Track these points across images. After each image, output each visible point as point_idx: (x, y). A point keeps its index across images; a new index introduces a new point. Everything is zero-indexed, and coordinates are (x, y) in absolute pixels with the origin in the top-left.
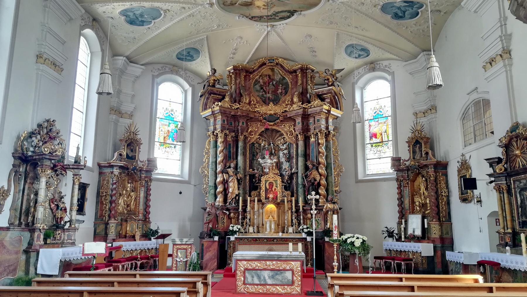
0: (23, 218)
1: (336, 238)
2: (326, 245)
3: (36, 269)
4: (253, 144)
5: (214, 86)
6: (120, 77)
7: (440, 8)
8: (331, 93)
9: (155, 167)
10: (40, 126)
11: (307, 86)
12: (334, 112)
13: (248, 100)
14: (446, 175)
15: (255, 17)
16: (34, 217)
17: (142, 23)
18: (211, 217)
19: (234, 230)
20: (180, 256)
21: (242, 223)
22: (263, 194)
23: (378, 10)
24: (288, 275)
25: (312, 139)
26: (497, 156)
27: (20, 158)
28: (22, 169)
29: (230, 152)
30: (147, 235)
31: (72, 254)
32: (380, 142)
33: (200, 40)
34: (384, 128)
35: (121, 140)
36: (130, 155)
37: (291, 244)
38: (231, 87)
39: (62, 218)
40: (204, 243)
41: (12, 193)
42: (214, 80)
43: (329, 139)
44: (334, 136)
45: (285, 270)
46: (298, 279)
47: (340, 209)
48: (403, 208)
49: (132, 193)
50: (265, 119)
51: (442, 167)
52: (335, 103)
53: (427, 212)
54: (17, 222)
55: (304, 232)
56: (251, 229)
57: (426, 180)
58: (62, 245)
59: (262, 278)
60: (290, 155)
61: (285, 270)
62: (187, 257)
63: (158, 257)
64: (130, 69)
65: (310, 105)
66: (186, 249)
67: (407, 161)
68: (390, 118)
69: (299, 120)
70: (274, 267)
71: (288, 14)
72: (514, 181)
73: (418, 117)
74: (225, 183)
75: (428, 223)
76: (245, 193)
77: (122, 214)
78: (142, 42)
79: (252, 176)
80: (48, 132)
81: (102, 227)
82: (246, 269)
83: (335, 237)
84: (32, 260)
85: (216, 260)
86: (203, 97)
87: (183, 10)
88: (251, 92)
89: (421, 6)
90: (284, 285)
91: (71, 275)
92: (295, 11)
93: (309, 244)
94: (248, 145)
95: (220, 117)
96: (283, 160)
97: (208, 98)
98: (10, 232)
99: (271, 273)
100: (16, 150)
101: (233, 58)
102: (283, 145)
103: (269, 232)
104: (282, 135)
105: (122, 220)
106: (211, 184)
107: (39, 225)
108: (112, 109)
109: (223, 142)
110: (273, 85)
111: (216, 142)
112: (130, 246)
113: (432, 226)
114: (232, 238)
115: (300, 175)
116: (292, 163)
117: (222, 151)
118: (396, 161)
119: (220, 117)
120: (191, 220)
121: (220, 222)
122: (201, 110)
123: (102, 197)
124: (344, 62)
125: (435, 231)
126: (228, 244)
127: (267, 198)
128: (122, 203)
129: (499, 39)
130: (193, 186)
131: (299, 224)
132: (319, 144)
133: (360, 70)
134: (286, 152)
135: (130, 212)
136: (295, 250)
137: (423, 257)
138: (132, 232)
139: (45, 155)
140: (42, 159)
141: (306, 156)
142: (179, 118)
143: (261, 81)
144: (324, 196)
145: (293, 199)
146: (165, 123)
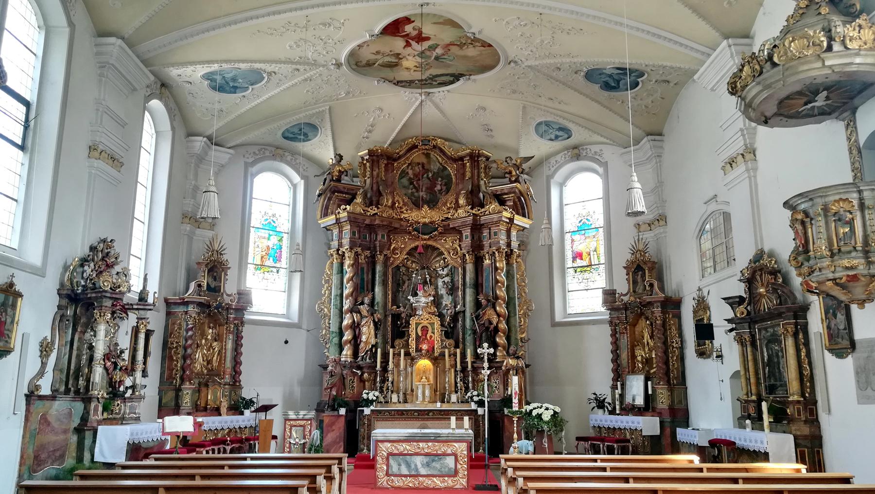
0: (71, 382)
1: (517, 409)
2: (506, 420)
3: (93, 456)
4: (398, 268)
5: (339, 180)
6: (197, 166)
7: (667, 78)
8: (514, 192)
9: (249, 303)
10: (93, 249)
11: (479, 182)
12: (519, 220)
13: (390, 202)
14: (678, 317)
15: (402, 82)
16: (88, 380)
17: (234, 90)
18: (335, 379)
19: (370, 398)
20: (296, 437)
21: (381, 388)
22: (413, 344)
23: (581, 77)
24: (450, 461)
25: (487, 262)
26: (738, 295)
27: (68, 297)
28: (69, 312)
29: (362, 280)
30: (237, 408)
31: (142, 434)
32: (587, 266)
33: (320, 112)
34: (593, 245)
35: (198, 263)
36: (212, 286)
37: (453, 418)
38: (365, 181)
39: (121, 382)
40: (325, 419)
41: (56, 346)
42: (340, 171)
43: (511, 261)
44: (519, 256)
45: (445, 454)
46: (463, 467)
47: (527, 366)
48: (619, 366)
49: (215, 344)
50: (415, 230)
51: (673, 305)
52: (521, 208)
53: (652, 371)
54: (63, 389)
55: (473, 401)
56: (395, 397)
57: (651, 324)
58: (122, 420)
59: (413, 466)
60: (453, 285)
61: (445, 454)
62: (304, 438)
63: (257, 438)
64: (211, 152)
65: (483, 210)
66: (304, 426)
67: (625, 295)
68: (601, 230)
69: (467, 232)
70: (430, 451)
71: (451, 79)
72: (760, 330)
73: (641, 230)
74: (355, 327)
75: (653, 387)
76: (385, 342)
77: (200, 374)
78: (233, 116)
79: (396, 317)
80: (104, 255)
81: (171, 394)
82: (390, 454)
83: (515, 408)
84: (88, 442)
85: (342, 443)
86: (323, 197)
87: (296, 72)
88: (395, 190)
89: (642, 74)
90: (443, 476)
91: (156, 459)
92: (462, 75)
93: (480, 419)
94: (390, 270)
95: (349, 227)
96: (443, 291)
97: (330, 199)
98: (57, 403)
99: (425, 459)
100: (62, 285)
101: (367, 138)
102: (443, 269)
103: (422, 401)
104: (442, 254)
105: (200, 384)
106: (334, 328)
107: (96, 392)
108: (184, 216)
109: (352, 265)
110: (428, 178)
111: (342, 264)
112: (214, 423)
113: (659, 391)
114: (367, 411)
115: (468, 314)
116: (457, 296)
117: (351, 279)
118: (610, 296)
119: (347, 228)
120: (301, 383)
121: (347, 387)
122: (319, 216)
123: (171, 349)
124: (534, 146)
125: (663, 401)
126: (360, 419)
127: (418, 350)
128: (201, 359)
129: (740, 133)
130: (304, 332)
131: (467, 389)
132: (496, 269)
133: (558, 158)
134: (447, 279)
135: (211, 373)
136: (460, 426)
137: (644, 436)
138: (215, 402)
139: (106, 292)
140: (101, 297)
141: (478, 286)
142: (284, 225)
143: (410, 172)
144: (504, 348)
145: (458, 351)
146: (263, 235)
